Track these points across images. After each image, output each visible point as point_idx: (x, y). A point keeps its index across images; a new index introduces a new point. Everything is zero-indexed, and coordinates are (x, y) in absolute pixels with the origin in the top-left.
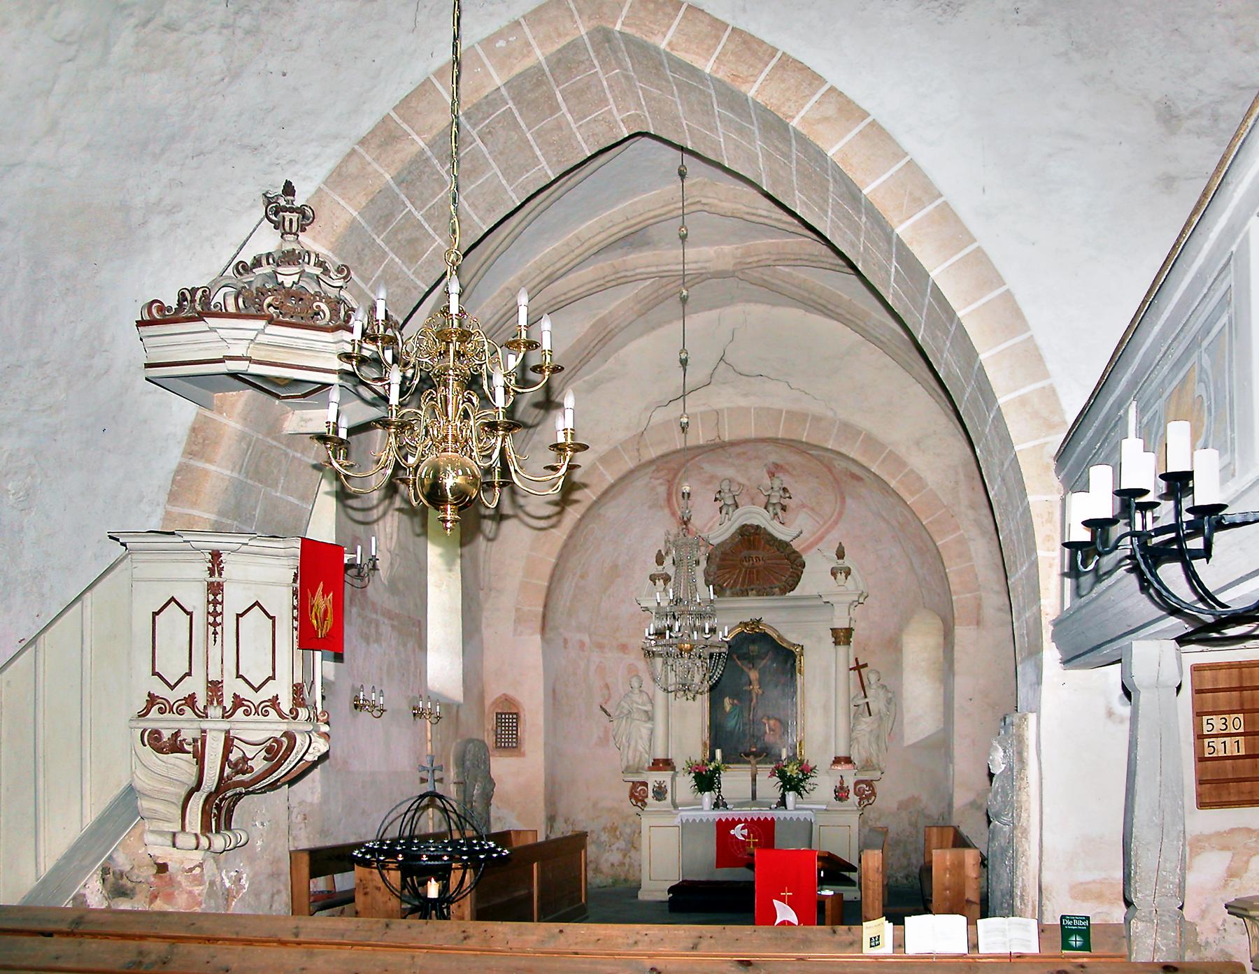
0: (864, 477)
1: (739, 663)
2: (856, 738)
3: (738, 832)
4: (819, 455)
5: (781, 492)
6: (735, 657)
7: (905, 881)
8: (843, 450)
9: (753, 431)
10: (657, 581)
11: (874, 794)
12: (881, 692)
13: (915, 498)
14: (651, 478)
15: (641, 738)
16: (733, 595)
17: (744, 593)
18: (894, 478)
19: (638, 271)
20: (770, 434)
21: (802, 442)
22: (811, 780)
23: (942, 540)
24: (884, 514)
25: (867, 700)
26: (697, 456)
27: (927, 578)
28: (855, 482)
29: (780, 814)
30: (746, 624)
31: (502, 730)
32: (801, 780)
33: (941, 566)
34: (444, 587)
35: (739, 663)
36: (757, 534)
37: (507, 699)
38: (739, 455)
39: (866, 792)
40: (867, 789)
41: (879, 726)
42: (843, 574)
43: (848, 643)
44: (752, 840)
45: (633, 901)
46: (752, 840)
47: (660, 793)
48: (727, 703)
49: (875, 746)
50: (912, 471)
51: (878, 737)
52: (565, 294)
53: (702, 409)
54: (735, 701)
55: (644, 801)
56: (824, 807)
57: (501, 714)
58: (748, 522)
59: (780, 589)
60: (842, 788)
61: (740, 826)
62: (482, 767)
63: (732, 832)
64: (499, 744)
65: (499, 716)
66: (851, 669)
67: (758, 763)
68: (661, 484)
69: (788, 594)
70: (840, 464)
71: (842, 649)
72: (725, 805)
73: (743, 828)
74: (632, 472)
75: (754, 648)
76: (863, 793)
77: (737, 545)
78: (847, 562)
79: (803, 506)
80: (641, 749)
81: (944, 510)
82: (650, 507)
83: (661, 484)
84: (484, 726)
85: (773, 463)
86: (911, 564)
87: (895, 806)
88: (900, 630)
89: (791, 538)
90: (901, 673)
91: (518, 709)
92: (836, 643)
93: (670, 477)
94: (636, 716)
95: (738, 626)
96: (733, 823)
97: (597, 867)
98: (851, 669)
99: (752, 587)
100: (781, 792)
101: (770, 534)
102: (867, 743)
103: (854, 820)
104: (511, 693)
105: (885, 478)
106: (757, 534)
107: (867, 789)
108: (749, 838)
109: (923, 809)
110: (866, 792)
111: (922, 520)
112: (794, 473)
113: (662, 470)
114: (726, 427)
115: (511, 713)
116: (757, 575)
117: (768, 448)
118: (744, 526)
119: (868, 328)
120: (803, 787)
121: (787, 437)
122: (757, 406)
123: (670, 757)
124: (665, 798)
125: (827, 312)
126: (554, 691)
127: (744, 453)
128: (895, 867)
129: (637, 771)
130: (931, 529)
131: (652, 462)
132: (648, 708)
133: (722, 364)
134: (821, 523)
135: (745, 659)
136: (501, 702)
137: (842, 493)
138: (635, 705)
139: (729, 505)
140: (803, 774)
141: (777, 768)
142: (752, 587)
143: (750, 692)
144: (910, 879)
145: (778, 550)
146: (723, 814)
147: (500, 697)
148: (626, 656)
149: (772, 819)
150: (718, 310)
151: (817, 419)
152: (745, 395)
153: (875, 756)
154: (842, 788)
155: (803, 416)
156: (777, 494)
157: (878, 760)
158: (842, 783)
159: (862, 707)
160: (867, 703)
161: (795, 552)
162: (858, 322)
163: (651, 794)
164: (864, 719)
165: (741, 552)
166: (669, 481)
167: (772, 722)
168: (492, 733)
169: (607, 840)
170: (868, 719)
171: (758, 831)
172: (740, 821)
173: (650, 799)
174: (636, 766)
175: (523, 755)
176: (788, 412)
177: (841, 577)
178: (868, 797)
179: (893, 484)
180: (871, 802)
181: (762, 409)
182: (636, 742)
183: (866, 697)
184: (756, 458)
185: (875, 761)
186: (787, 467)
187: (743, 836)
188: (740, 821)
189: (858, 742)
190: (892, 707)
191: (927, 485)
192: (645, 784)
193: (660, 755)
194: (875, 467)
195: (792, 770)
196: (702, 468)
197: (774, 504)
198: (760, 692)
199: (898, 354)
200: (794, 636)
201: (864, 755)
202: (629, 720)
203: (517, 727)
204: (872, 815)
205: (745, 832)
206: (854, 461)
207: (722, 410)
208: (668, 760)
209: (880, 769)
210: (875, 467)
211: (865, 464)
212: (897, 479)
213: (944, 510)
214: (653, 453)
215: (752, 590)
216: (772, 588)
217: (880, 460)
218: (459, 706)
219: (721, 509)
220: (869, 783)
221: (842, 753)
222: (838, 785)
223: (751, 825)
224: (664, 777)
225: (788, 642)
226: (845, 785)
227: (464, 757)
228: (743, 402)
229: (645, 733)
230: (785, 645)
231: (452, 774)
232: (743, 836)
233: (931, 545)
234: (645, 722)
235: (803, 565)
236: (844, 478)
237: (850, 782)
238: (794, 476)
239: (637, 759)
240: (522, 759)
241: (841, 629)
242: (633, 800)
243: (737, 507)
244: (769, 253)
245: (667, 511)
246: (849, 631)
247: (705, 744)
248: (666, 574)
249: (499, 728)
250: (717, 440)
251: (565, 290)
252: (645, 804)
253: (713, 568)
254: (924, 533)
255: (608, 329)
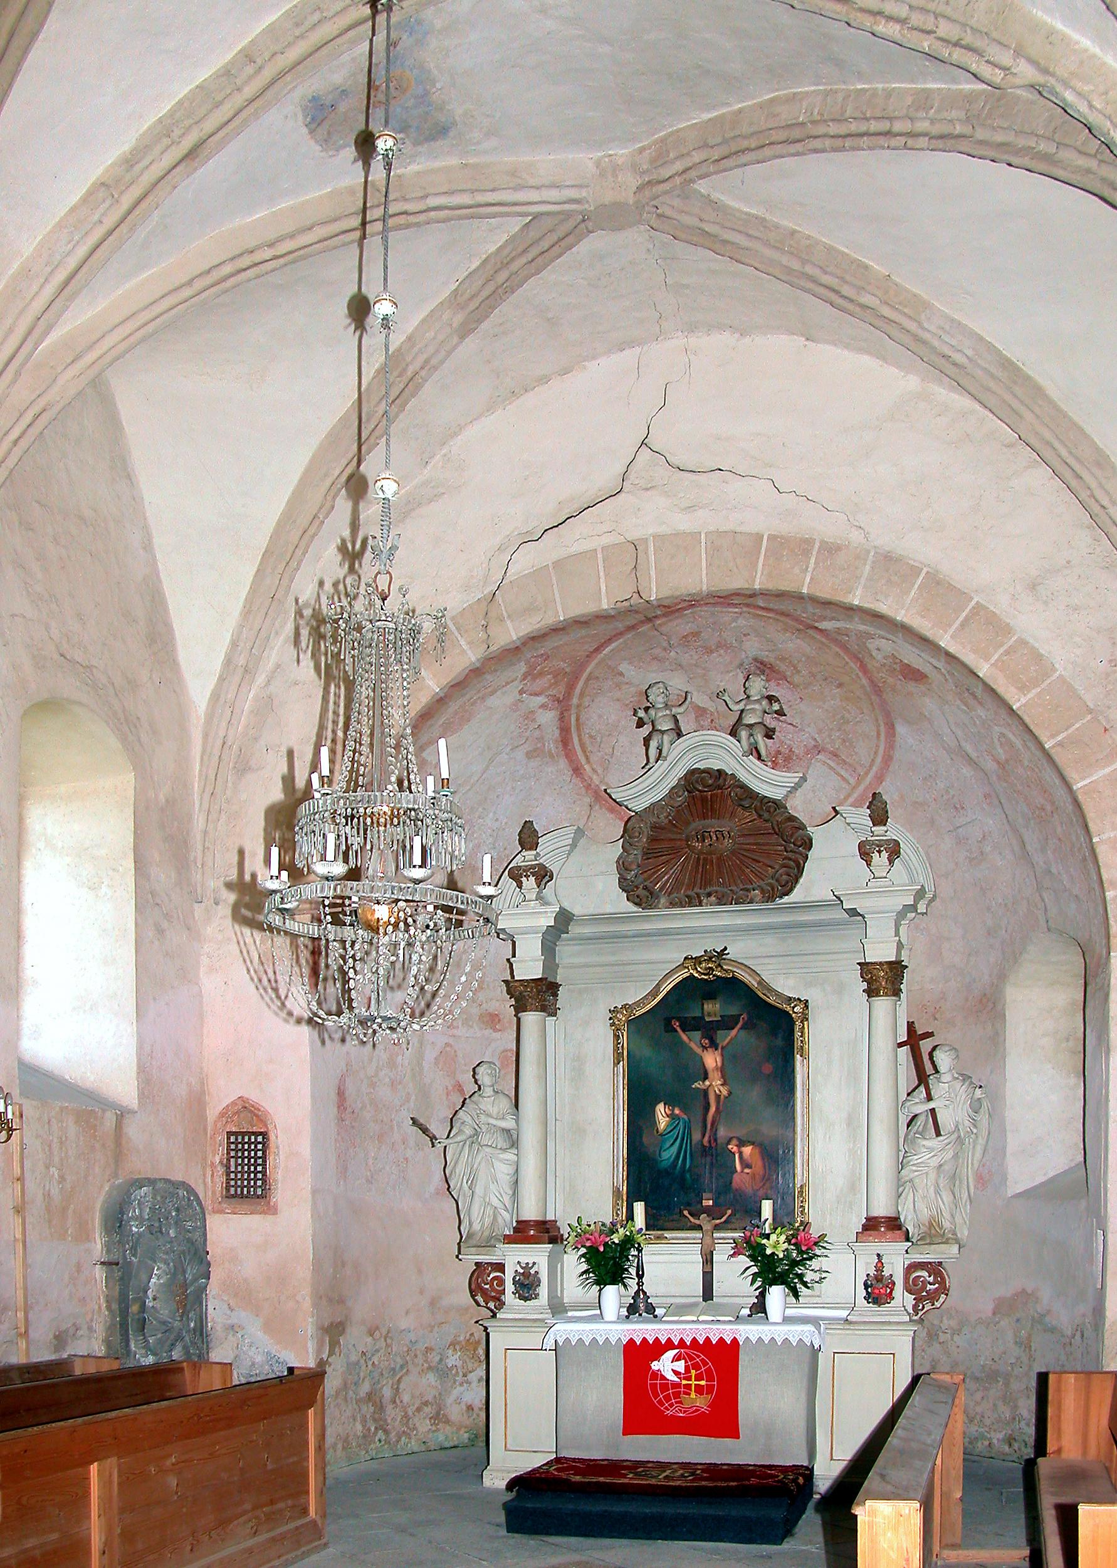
0: (926, 669)
1: (684, 1037)
2: (911, 1181)
3: (667, 1366)
4: (838, 631)
5: (765, 702)
6: (676, 1025)
7: (1006, 1448)
8: (883, 608)
9: (704, 580)
10: (524, 879)
11: (944, 1289)
12: (962, 1090)
13: (1030, 695)
14: (521, 692)
15: (495, 1180)
16: (672, 904)
17: (693, 901)
18: (987, 658)
19: (433, 202)
20: (737, 583)
21: (800, 597)
22: (815, 1264)
23: (1083, 779)
24: (969, 748)
25: (931, 1105)
26: (609, 641)
27: (1054, 870)
28: (912, 686)
29: (748, 1332)
30: (697, 960)
31: (237, 1165)
32: (794, 1263)
33: (1081, 832)
34: (104, 889)
35: (684, 1037)
36: (720, 787)
37: (246, 1108)
38: (687, 640)
39: (929, 1287)
40: (931, 1279)
41: (956, 1156)
42: (885, 855)
43: (897, 993)
44: (693, 1382)
45: (471, 1489)
46: (693, 1382)
47: (527, 1286)
48: (662, 1114)
49: (946, 1197)
50: (1022, 642)
51: (953, 1177)
52: (271, 245)
53: (606, 540)
54: (677, 1111)
55: (499, 1299)
56: (843, 1314)
57: (236, 1134)
58: (701, 766)
59: (763, 891)
60: (879, 1278)
61: (671, 1354)
62: (172, 1233)
63: (655, 1365)
64: (232, 1191)
65: (232, 1139)
66: (900, 1045)
67: (717, 1228)
68: (543, 706)
69: (778, 900)
70: (882, 647)
71: (882, 1004)
72: (650, 1309)
73: (677, 1358)
74: (476, 672)
75: (713, 1009)
76: (923, 1288)
77: (679, 810)
78: (892, 831)
79: (818, 749)
80: (495, 1202)
81: (1089, 717)
82: (529, 755)
83: (543, 706)
84: (205, 1159)
85: (755, 660)
86: (1023, 844)
87: (989, 1307)
88: (1002, 977)
89: (784, 791)
90: (1004, 1058)
91: (266, 1126)
92: (871, 992)
93: (560, 691)
94: (485, 1139)
95: (682, 966)
96: (657, 1349)
97: (438, 1413)
98: (900, 1045)
99: (708, 890)
100: (758, 1284)
101: (743, 787)
102: (932, 1190)
103: (902, 1343)
104: (254, 1096)
105: (969, 658)
106: (720, 787)
107: (931, 1279)
108: (689, 1378)
109: (1042, 1316)
110: (929, 1287)
111: (1043, 739)
112: (796, 679)
113: (541, 674)
114: (653, 573)
115: (253, 1133)
116: (719, 867)
117: (741, 622)
118: (693, 772)
119: (926, 336)
120: (800, 1277)
121: (771, 586)
122: (712, 528)
123: (550, 1217)
124: (537, 1296)
125: (840, 301)
126: (341, 1094)
127: (696, 634)
128: (987, 1422)
129: (488, 1244)
130: (1060, 757)
131: (513, 652)
132: (509, 1124)
133: (645, 452)
134: (852, 781)
135: (695, 1029)
136: (237, 1113)
137: (888, 715)
138: (483, 1118)
139: (663, 732)
140: (800, 1252)
141: (747, 1240)
142: (708, 890)
143: (705, 1093)
144: (1016, 1445)
145: (760, 816)
146: (643, 1330)
147: (234, 1103)
148: (498, 1035)
149: (735, 1340)
150: (637, 350)
151: (830, 549)
152: (690, 509)
153: (946, 1214)
154: (879, 1278)
155: (802, 546)
156: (757, 706)
157: (953, 1222)
158: (880, 1267)
159: (922, 1119)
160: (933, 1111)
161: (792, 819)
162: (906, 323)
163: (509, 1287)
164: (925, 1142)
165: (688, 823)
166: (559, 701)
167: (747, 1150)
168: (221, 1170)
169: (459, 1363)
170: (934, 1143)
171: (705, 1363)
172: (670, 1345)
173: (509, 1297)
174: (486, 1234)
175: (272, 1210)
176: (772, 538)
177: (880, 860)
178: (932, 1297)
179: (984, 670)
180: (937, 1304)
181: (719, 533)
182: (486, 1188)
183: (929, 1098)
184: (719, 645)
185: (947, 1225)
186: (782, 667)
187: (676, 1373)
188: (670, 1345)
189: (914, 1188)
190: (983, 1118)
191: (1054, 670)
192: (500, 1267)
193: (530, 1213)
194: (947, 637)
195: (777, 1244)
196: (621, 674)
197: (750, 726)
198: (725, 1092)
199: (988, 389)
200: (791, 982)
201: (925, 1214)
202: (475, 1146)
203: (264, 1158)
204: (946, 1323)
205: (680, 1366)
206: (905, 630)
207: (645, 541)
208: (544, 1222)
209: (957, 1241)
210: (947, 637)
211: (929, 634)
212: (992, 661)
213: (1089, 717)
214: (512, 632)
215: (709, 895)
216: (748, 890)
217: (958, 622)
218: (122, 1114)
219: (647, 741)
220: (935, 1269)
221: (881, 1209)
222: (872, 1272)
223: (692, 1350)
224: (537, 1255)
225: (778, 995)
226: (886, 1273)
227: (122, 1213)
228: (684, 523)
229: (503, 1171)
230: (771, 1000)
231: (99, 1246)
232: (676, 1373)
233: (1061, 792)
234: (504, 1150)
235: (808, 844)
236: (890, 680)
237: (895, 1268)
238: (796, 686)
239: (488, 1221)
240: (270, 1218)
241: (881, 964)
242: (479, 1298)
243: (680, 735)
244: (706, 146)
245: (563, 763)
246: (896, 969)
247: (617, 1193)
248: (542, 867)
249: (233, 1160)
250: (635, 600)
251: (272, 236)
252: (501, 1304)
253: (636, 854)
254: (1049, 776)
255: (409, 374)
